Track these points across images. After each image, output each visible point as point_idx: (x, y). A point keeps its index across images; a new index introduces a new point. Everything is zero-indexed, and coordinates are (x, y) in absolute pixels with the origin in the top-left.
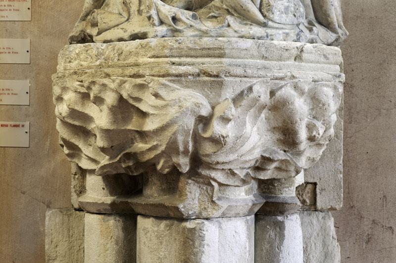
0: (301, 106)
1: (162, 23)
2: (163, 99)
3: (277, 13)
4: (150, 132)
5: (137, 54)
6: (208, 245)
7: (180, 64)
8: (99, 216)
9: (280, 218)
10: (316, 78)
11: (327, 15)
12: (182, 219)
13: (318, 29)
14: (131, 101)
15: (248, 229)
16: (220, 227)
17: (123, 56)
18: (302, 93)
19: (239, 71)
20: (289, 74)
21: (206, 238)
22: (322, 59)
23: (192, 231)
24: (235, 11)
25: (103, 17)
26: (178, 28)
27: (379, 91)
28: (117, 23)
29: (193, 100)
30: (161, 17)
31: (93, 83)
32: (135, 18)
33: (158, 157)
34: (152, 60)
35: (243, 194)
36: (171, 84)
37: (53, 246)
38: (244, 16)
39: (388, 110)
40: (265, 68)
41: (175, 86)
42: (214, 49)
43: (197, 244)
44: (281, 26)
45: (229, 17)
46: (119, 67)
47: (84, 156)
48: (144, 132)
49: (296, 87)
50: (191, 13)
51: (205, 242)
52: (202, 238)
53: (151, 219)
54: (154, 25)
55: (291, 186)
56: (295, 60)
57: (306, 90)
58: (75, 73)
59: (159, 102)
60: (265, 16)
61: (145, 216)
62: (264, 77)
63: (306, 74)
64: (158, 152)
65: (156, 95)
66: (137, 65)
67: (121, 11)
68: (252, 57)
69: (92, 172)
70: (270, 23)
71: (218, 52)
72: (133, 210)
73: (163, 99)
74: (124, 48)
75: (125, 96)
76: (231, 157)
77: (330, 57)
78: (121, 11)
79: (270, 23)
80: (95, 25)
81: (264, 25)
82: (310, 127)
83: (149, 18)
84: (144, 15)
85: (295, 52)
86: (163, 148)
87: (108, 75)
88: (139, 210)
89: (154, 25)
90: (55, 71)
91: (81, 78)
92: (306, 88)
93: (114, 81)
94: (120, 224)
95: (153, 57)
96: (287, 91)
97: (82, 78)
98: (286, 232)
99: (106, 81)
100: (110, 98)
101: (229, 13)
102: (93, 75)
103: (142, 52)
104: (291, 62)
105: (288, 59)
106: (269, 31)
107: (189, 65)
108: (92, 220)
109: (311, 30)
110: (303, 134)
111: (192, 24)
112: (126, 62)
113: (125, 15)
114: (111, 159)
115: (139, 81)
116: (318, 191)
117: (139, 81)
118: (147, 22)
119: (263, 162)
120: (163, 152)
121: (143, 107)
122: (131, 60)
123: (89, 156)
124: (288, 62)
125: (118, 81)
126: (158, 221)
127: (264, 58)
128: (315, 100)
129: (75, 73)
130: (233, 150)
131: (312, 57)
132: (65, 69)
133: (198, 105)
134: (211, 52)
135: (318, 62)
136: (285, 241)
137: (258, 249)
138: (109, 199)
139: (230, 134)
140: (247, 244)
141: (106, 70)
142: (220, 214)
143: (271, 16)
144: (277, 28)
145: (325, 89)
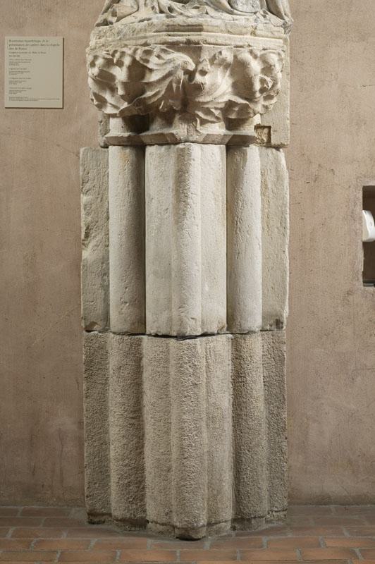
0: (255, 67)
1: (161, 12)
2: (163, 59)
3: (240, 4)
4: (154, 82)
5: (145, 30)
6: (194, 160)
7: (174, 36)
8: (120, 147)
9: (245, 148)
10: (265, 47)
11: (277, 7)
12: (177, 142)
13: (269, 15)
14: (141, 62)
15: (222, 154)
16: (202, 150)
17: (135, 32)
18: (255, 57)
19: (212, 40)
20: (247, 44)
21: (193, 154)
22: (270, 35)
23: (182, 150)
24: (212, 3)
25: (120, 9)
26: (173, 14)
27: (323, 67)
28: (130, 12)
29: (183, 59)
30: (161, 7)
31: (115, 52)
32: (142, 9)
33: (159, 101)
34: (155, 34)
35: (218, 128)
36: (168, 49)
37: (85, 173)
38: (218, 7)
39: (329, 82)
40: (230, 39)
41: (171, 50)
42: (196, 25)
43: (186, 159)
44: (239, 13)
45: (207, 7)
46: (133, 39)
47: (108, 105)
48: (151, 83)
49: (251, 52)
50: (181, 4)
51: (192, 157)
52: (190, 155)
53: (156, 146)
54: (156, 13)
55: (251, 124)
56: (251, 34)
57: (259, 55)
58: (103, 45)
59: (161, 61)
60: (232, 7)
61: (151, 145)
62: (229, 45)
63: (258, 44)
64: (160, 96)
65: (159, 57)
66: (145, 37)
67: (133, 4)
68: (222, 31)
69: (114, 116)
70: (235, 11)
71: (198, 27)
72: (142, 142)
73: (163, 59)
74: (136, 27)
75: (138, 58)
76: (208, 99)
77: (276, 33)
78: (133, 4)
79: (235, 11)
80: (114, 14)
81: (231, 13)
82: (263, 81)
83: (153, 8)
84: (149, 6)
85: (250, 29)
86: (163, 93)
87: (126, 46)
88: (146, 141)
89: (156, 13)
90: (88, 45)
91: (107, 49)
92: (259, 54)
93: (130, 49)
94: (134, 152)
95: (157, 31)
96: (245, 55)
97: (109, 48)
98: (248, 157)
99: (124, 49)
100: (127, 61)
101: (207, 4)
102: (115, 46)
103: (149, 29)
104: (248, 36)
105: (246, 34)
106: (235, 17)
107: (179, 36)
108: (113, 150)
109: (265, 17)
110: (257, 86)
111: (182, 12)
112: (138, 36)
113: (135, 7)
114: (129, 104)
115: (147, 48)
116: (272, 132)
117: (147, 48)
118: (151, 12)
119: (230, 105)
120: (163, 96)
121: (150, 66)
122: (142, 34)
123: (114, 104)
124: (245, 36)
125: (133, 49)
126: (160, 147)
127: (229, 32)
128: (268, 69)
129: (103, 45)
130: (209, 93)
131: (263, 33)
132: (96, 44)
133: (186, 63)
134: (194, 27)
135: (267, 37)
136: (247, 163)
137: (229, 169)
138: (126, 134)
139: (207, 82)
140: (221, 164)
141: (126, 42)
142: (202, 140)
143: (236, 6)
144: (240, 15)
145: (272, 55)
